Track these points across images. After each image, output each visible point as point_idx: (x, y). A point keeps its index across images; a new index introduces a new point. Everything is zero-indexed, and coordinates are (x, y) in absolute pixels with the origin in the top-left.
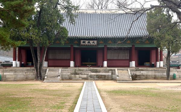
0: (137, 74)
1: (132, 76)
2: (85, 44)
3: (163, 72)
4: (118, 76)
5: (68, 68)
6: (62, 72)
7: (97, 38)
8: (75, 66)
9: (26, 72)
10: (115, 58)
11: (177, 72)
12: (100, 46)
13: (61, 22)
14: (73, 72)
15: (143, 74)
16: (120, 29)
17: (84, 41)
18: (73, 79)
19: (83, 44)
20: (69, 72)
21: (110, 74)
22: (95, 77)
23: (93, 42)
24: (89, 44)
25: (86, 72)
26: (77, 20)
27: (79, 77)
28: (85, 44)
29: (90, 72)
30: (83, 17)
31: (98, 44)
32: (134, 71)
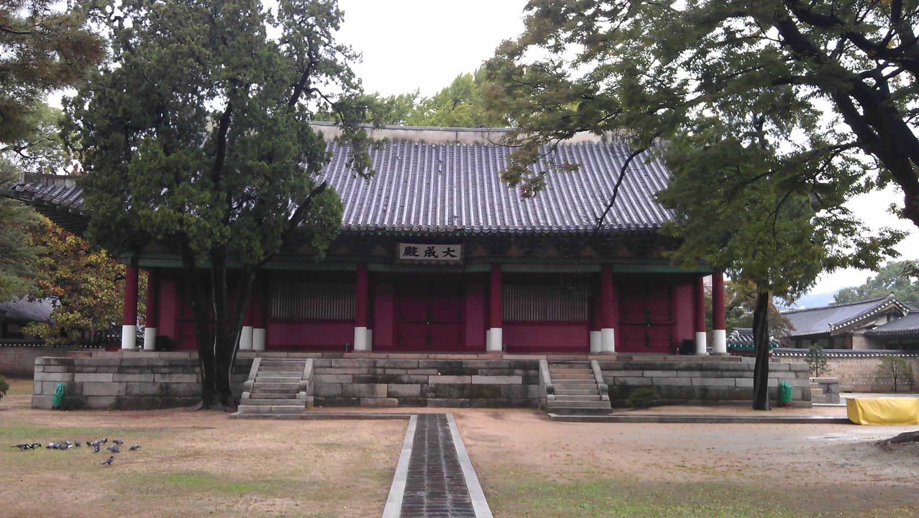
0: (631, 381)
1: (611, 393)
2: (413, 257)
3: (738, 374)
4: (551, 391)
5: (347, 355)
6: (318, 370)
7: (462, 235)
8: (376, 346)
9: (167, 370)
10: (535, 317)
11: (792, 375)
12: (474, 269)
13: (315, 168)
14: (365, 370)
15: (655, 382)
16: (555, 200)
17: (412, 245)
18: (363, 401)
19: (408, 257)
20: (344, 371)
21: (517, 380)
22: (455, 393)
23: (448, 252)
24: (432, 258)
25: (419, 371)
26: (379, 161)
27: (390, 395)
28: (413, 257)
29: (435, 371)
30: (409, 158)
31: (467, 258)
32: (617, 370)
